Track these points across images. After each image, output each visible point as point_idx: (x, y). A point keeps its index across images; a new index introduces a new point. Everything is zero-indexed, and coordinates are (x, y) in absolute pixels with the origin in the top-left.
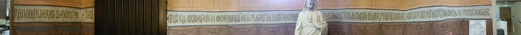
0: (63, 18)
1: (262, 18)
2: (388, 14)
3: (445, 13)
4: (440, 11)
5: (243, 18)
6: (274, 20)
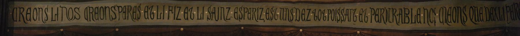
0: (256, 19)
3: (480, 14)
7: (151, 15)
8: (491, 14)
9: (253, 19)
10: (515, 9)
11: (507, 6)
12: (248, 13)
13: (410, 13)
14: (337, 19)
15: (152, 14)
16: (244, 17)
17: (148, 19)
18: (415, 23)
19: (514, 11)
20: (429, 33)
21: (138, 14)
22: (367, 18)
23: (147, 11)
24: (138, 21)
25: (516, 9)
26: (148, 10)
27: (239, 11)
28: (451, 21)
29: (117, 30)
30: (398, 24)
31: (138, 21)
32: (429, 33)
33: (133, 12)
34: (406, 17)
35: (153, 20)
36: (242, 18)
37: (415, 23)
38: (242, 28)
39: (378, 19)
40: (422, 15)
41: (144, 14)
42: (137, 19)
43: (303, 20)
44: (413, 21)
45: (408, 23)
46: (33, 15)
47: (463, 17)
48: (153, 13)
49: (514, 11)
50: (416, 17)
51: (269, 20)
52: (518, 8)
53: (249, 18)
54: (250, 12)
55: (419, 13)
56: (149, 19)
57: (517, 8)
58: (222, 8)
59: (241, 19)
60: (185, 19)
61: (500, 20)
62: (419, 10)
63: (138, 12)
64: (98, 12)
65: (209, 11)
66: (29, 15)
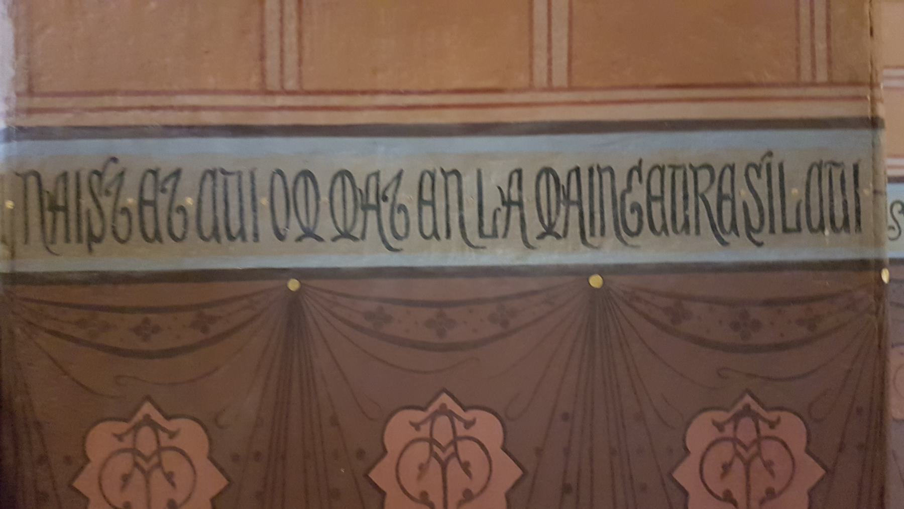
0: (713, 227)
2: (668, 172)
4: (704, 175)
5: (153, 204)
6: (150, 231)
7: (396, 215)
15: (399, 211)
16: (858, 221)
17: (239, 240)
22: (403, 214)
23: (658, 194)
26: (156, 195)
28: (798, 223)
29: (596, 281)
30: (52, 247)
33: (721, 197)
34: (178, 212)
36: (762, 222)
39: (435, 223)
44: (791, 223)
45: (799, 229)
48: (182, 209)
51: (213, 241)
53: (207, 232)
56: (737, 234)
59: (99, 240)
60: (203, 238)
61: (786, 230)
62: (574, 176)
64: (662, 192)
65: (96, 191)
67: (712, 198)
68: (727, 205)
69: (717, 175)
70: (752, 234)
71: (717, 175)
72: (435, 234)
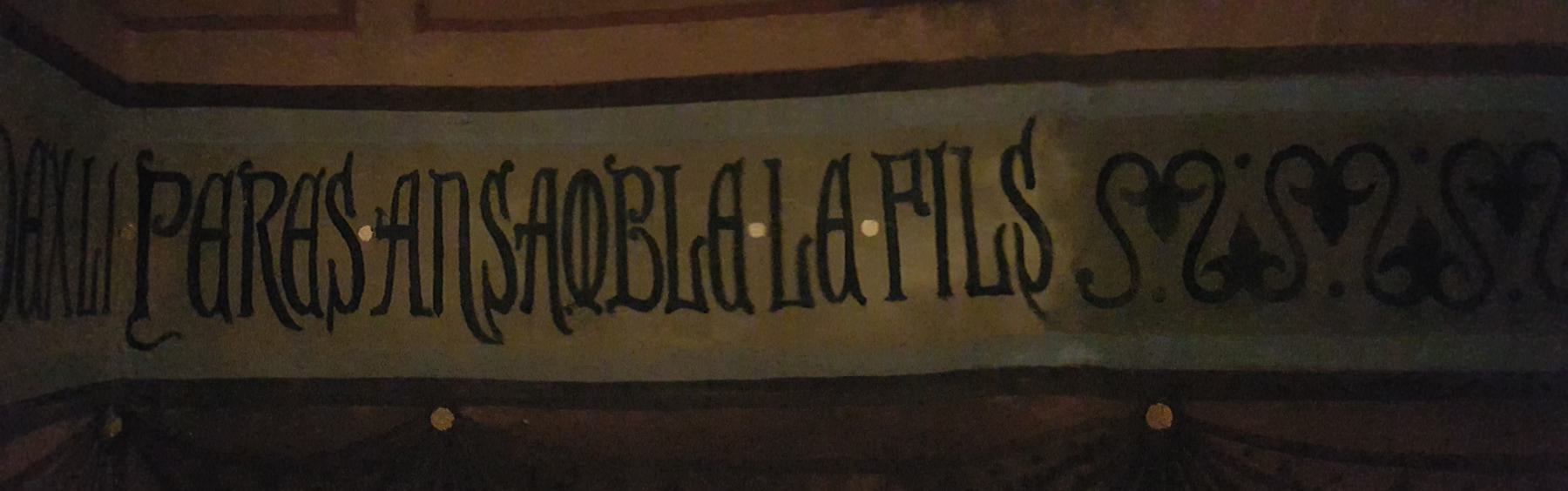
1: (311, 234)
4: (264, 193)
8: (549, 230)
9: (247, 309)
10: (248, 216)
11: (619, 165)
12: (200, 236)
13: (659, 211)
14: (488, 290)
17: (850, 300)
18: (806, 301)
19: (236, 228)
20: (468, 411)
21: (332, 265)
24: (330, 327)
25: (262, 227)
27: (325, 222)
31: (330, 327)
32: (468, 411)
33: (290, 235)
35: (838, 305)
37: (806, 301)
38: (1161, 416)
40: (757, 230)
41: (745, 205)
42: (324, 308)
43: (210, 304)
46: (107, 297)
47: (485, 267)
49: (236, 228)
50: (812, 251)
52: (281, 214)
54: (212, 221)
55: (726, 210)
57: (271, 212)
58: (446, 186)
63: (329, 236)
66: (306, 244)
67: (275, 228)
68: (301, 248)
69: (291, 188)
70: (494, 313)
71: (291, 188)
72: (222, 305)
